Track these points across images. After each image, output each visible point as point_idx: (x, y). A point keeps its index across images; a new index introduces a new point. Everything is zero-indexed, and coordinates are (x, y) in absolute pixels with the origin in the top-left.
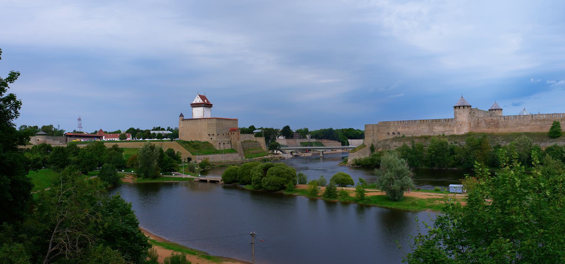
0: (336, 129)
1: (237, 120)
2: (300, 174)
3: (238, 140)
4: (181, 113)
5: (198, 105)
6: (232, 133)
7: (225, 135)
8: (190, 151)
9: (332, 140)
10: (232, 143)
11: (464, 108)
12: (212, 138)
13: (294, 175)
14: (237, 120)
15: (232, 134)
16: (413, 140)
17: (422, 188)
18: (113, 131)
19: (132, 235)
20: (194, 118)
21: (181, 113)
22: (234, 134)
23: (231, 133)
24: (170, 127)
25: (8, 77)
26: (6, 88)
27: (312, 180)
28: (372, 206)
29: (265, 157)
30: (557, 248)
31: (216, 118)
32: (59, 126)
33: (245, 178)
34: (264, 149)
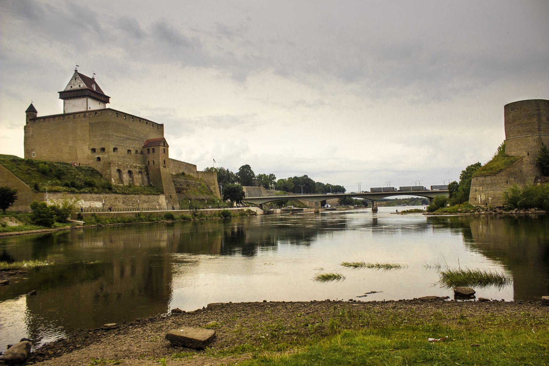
0: (328, 184)
1: (431, 186)
2: (220, 252)
3: (164, 167)
4: (31, 105)
5: (75, 93)
6: (151, 151)
7: (133, 152)
8: (377, 308)
9: (469, 195)
10: (150, 172)
11: (397, 211)
12: (99, 159)
13: (70, 240)
14: (431, 186)
15: (149, 152)
16: (91, 358)
17: (46, 228)
18: (410, 297)
19: (69, 347)
20: (72, 93)
21: (31, 105)
22: (154, 152)
23: (148, 150)
24: (208, 168)
25: (347, 301)
26: (87, 242)
27: (196, 337)
28: (188, 262)
29: (226, 209)
30: (120, 239)
31: (64, 106)
32: (360, 186)
33: (466, 225)
34: (543, 297)
